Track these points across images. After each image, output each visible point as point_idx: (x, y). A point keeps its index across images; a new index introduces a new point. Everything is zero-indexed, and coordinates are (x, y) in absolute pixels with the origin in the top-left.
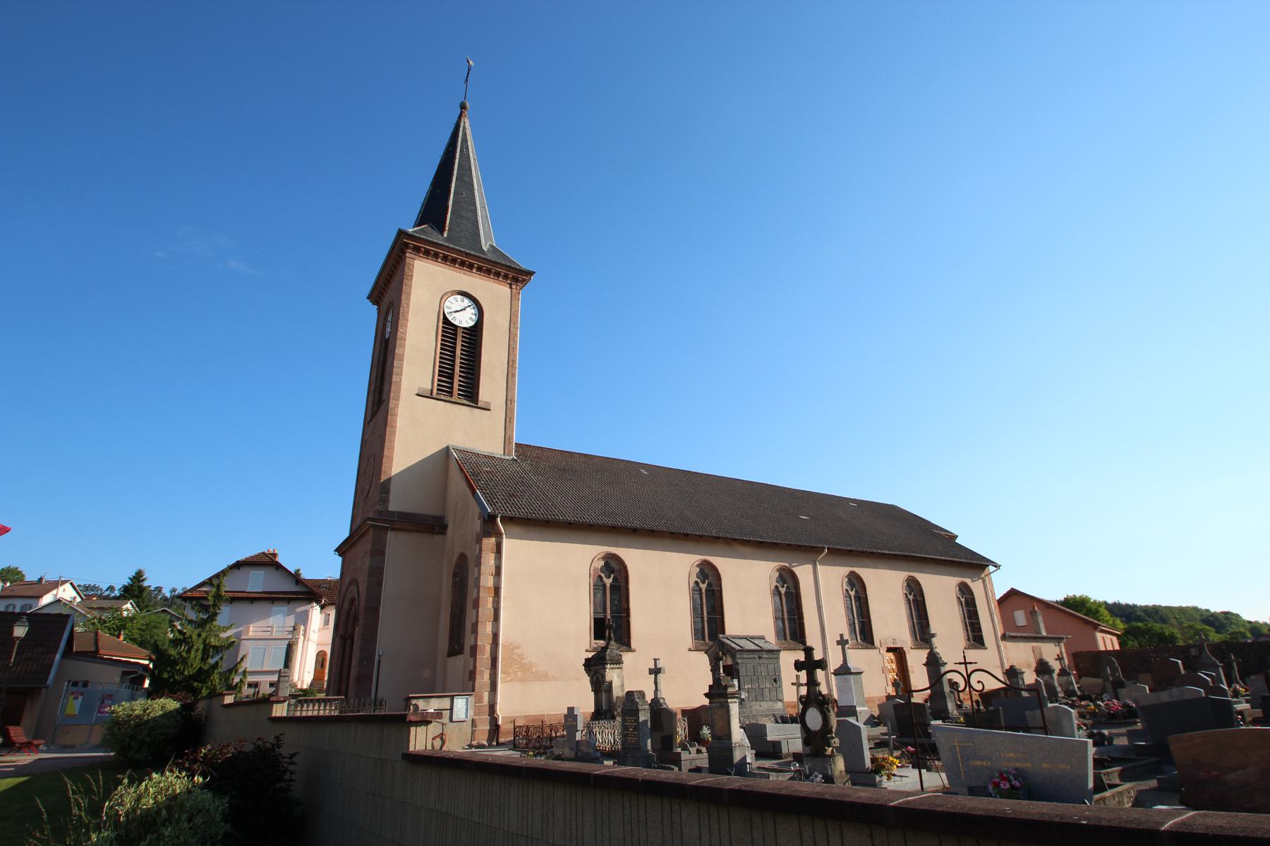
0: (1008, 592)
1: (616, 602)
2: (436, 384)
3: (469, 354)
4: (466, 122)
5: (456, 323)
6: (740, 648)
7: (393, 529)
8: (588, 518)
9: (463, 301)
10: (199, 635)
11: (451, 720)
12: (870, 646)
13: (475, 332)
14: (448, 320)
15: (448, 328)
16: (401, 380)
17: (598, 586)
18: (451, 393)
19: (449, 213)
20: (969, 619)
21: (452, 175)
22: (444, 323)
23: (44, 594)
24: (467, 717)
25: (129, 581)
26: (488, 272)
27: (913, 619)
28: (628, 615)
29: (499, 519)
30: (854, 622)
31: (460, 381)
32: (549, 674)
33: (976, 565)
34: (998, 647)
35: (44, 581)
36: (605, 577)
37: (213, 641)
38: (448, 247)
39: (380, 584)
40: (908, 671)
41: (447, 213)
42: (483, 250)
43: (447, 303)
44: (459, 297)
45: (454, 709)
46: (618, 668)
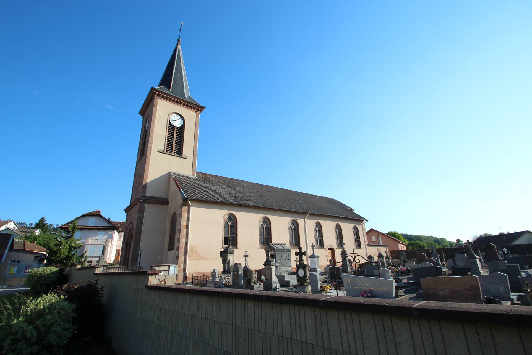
2: (166, 148)
4: (180, 47)
5: (174, 125)
7: (147, 203)
10: (67, 243)
13: (182, 129)
15: (171, 127)
18: (172, 152)
21: (174, 67)
22: (169, 125)
23: (2, 226)
25: (39, 221)
26: (187, 106)
29: (189, 200)
33: (360, 220)
34: (366, 248)
38: (171, 95)
39: (142, 223)
41: (171, 82)
43: (171, 117)
44: (176, 115)
45: (170, 271)
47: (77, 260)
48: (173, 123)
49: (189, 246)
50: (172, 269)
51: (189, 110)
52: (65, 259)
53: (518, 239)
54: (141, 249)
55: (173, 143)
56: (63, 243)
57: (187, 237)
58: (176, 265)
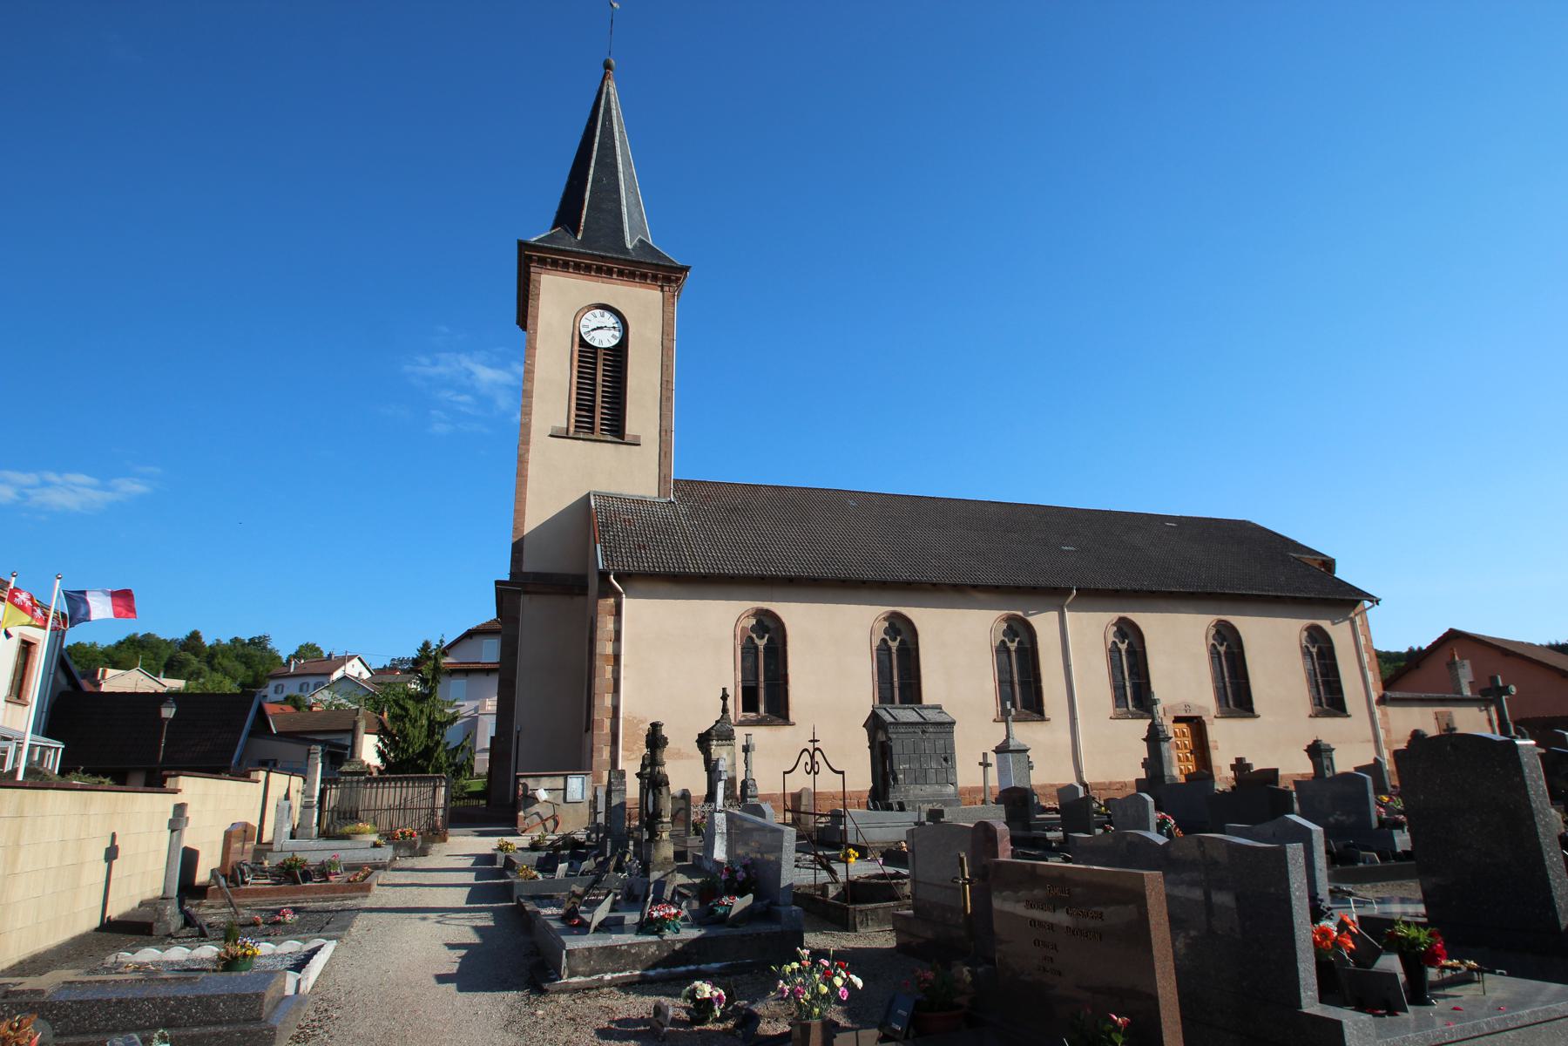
0: (1445, 635)
1: (772, 667)
2: (573, 421)
3: (615, 380)
4: (612, 87)
5: (596, 344)
6: (893, 720)
7: (527, 593)
8: (729, 569)
9: (603, 316)
10: (422, 712)
11: (565, 800)
12: (1247, 714)
13: (620, 351)
14: (585, 341)
15: (586, 350)
16: (530, 420)
17: (749, 650)
18: (592, 430)
19: (585, 209)
20: (1322, 676)
21: (590, 158)
22: (580, 346)
23: (334, 671)
24: (583, 798)
25: (417, 653)
26: (632, 275)
27: (1223, 678)
28: (786, 682)
29: (612, 576)
30: (1125, 683)
31: (602, 413)
32: (682, 751)
33: (1348, 600)
34: (1372, 714)
35: (333, 657)
36: (757, 637)
37: (438, 717)
38: (578, 253)
39: (515, 654)
40: (1208, 747)
41: (583, 209)
42: (627, 249)
43: (584, 322)
44: (598, 312)
45: (568, 789)
46: (728, 745)
47: (448, 758)
48: (590, 337)
49: (624, 718)
50: (574, 787)
51: (641, 287)
52: (420, 755)
53: (1307, 681)
54: (516, 728)
55: (594, 401)
56: (412, 711)
57: (616, 690)
58: (586, 774)
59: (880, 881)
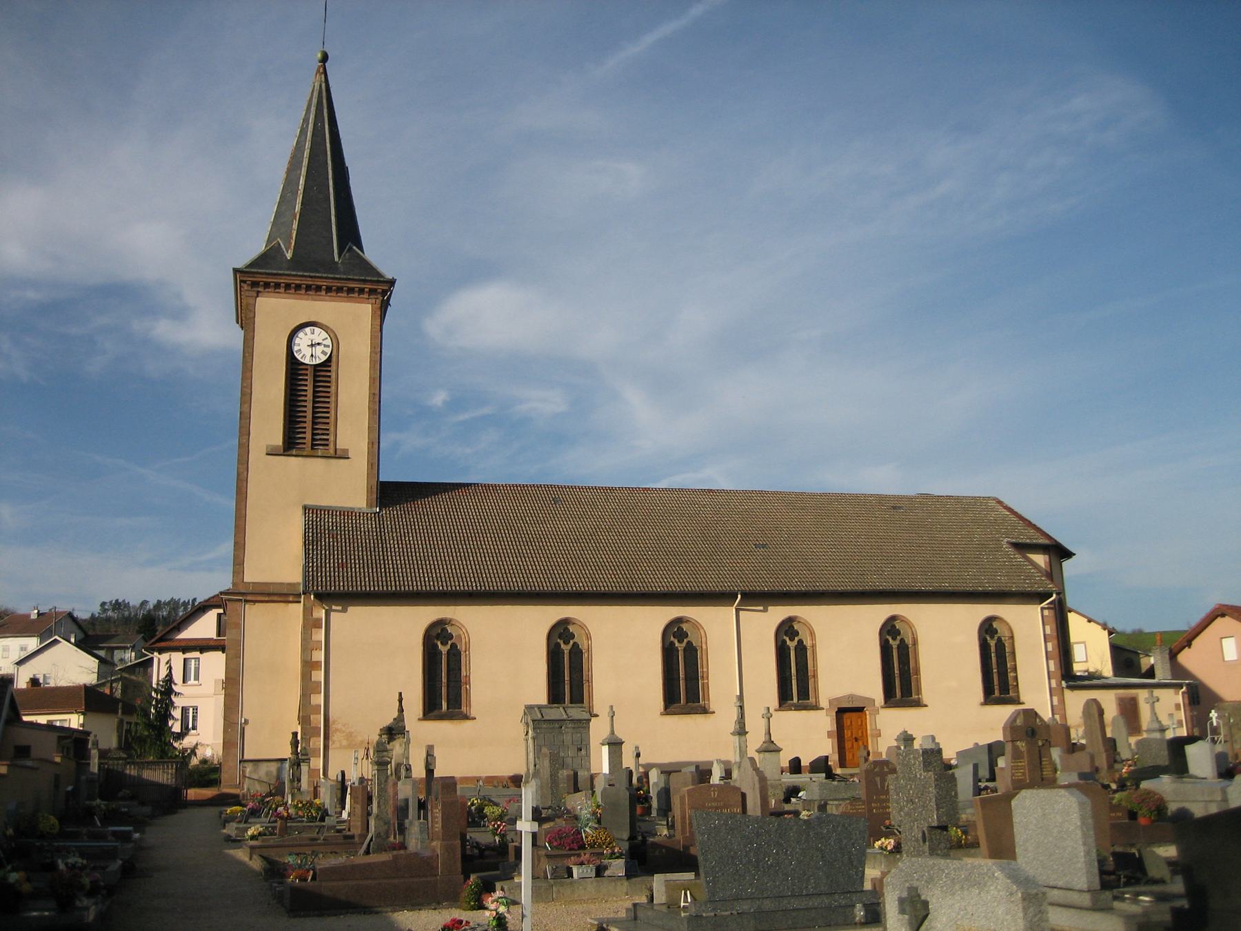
8: (918, 586)
48: (301, 355)
59: (62, 844)
